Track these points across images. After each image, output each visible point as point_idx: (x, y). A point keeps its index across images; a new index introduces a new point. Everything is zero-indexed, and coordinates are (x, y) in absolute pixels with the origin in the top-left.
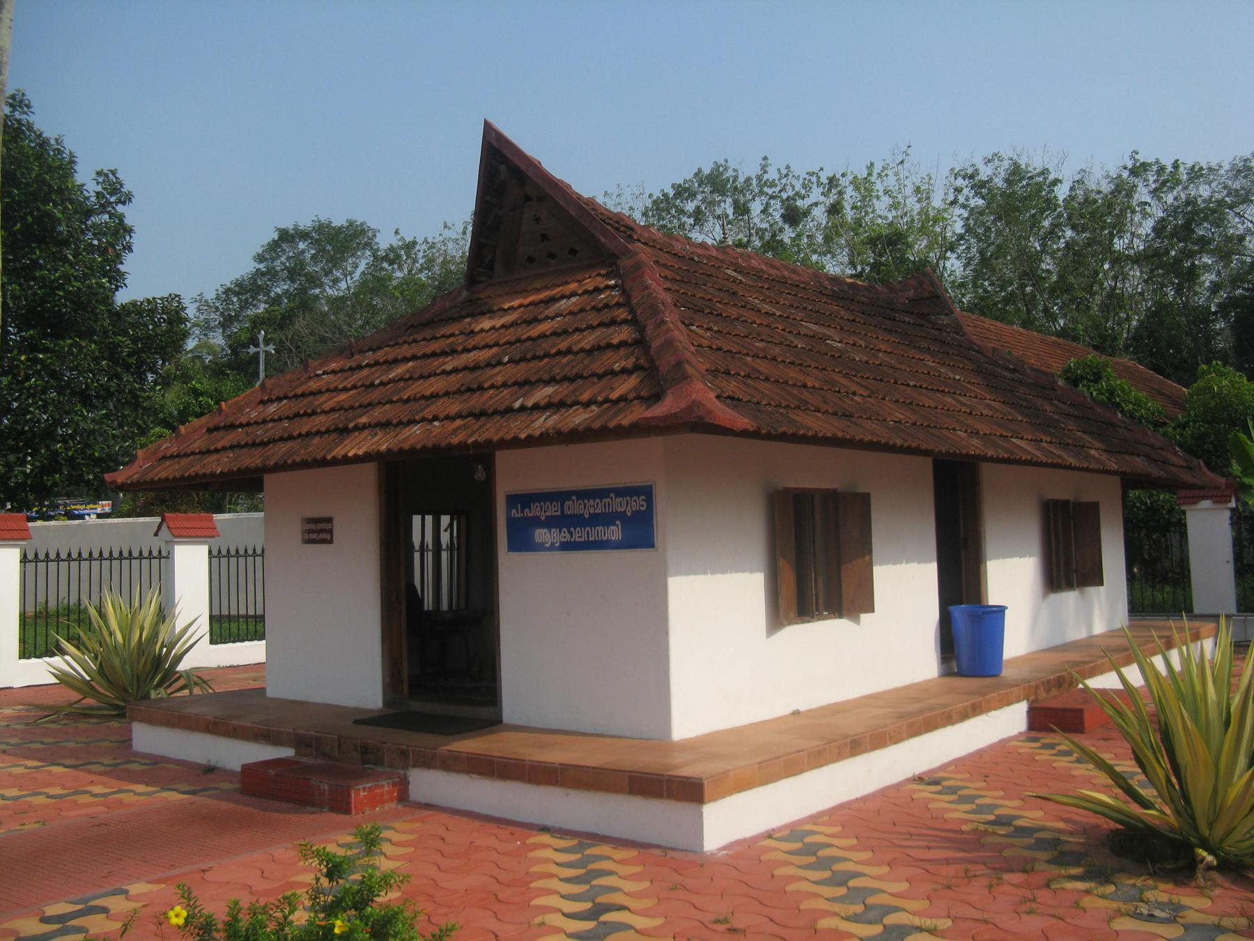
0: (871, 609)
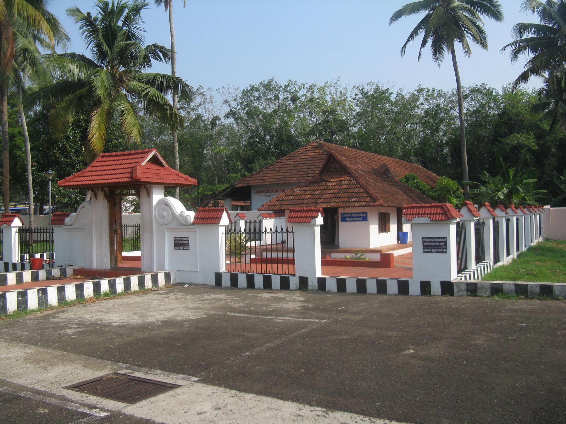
0: (390, 231)
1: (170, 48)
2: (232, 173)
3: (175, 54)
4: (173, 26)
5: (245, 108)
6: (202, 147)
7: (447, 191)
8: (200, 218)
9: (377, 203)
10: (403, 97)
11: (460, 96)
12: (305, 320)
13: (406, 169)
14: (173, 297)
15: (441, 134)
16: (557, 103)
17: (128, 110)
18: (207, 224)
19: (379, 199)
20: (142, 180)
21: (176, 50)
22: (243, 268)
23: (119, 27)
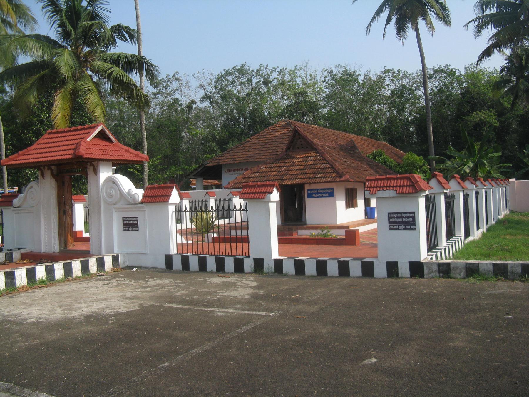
0: (357, 207)
1: (136, 29)
2: (208, 154)
3: (141, 35)
4: (138, 7)
5: (219, 92)
6: (179, 130)
7: (414, 167)
8: (149, 196)
9: (343, 179)
10: (370, 79)
11: (425, 77)
12: (251, 313)
13: (373, 146)
14: (115, 284)
15: (407, 114)
16: (518, 79)
17: (91, 90)
18: (155, 202)
19: (345, 175)
20: (85, 156)
21: (141, 31)
22: (195, 250)
23: (82, 7)
